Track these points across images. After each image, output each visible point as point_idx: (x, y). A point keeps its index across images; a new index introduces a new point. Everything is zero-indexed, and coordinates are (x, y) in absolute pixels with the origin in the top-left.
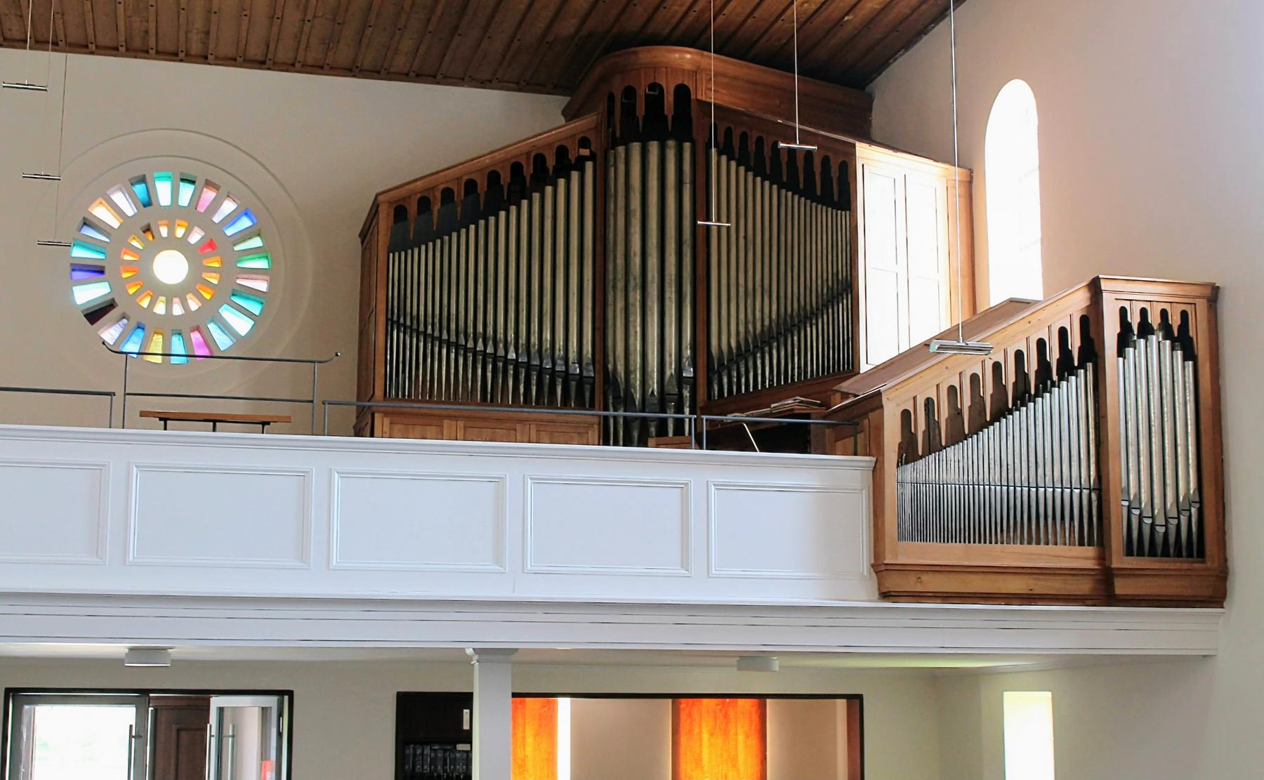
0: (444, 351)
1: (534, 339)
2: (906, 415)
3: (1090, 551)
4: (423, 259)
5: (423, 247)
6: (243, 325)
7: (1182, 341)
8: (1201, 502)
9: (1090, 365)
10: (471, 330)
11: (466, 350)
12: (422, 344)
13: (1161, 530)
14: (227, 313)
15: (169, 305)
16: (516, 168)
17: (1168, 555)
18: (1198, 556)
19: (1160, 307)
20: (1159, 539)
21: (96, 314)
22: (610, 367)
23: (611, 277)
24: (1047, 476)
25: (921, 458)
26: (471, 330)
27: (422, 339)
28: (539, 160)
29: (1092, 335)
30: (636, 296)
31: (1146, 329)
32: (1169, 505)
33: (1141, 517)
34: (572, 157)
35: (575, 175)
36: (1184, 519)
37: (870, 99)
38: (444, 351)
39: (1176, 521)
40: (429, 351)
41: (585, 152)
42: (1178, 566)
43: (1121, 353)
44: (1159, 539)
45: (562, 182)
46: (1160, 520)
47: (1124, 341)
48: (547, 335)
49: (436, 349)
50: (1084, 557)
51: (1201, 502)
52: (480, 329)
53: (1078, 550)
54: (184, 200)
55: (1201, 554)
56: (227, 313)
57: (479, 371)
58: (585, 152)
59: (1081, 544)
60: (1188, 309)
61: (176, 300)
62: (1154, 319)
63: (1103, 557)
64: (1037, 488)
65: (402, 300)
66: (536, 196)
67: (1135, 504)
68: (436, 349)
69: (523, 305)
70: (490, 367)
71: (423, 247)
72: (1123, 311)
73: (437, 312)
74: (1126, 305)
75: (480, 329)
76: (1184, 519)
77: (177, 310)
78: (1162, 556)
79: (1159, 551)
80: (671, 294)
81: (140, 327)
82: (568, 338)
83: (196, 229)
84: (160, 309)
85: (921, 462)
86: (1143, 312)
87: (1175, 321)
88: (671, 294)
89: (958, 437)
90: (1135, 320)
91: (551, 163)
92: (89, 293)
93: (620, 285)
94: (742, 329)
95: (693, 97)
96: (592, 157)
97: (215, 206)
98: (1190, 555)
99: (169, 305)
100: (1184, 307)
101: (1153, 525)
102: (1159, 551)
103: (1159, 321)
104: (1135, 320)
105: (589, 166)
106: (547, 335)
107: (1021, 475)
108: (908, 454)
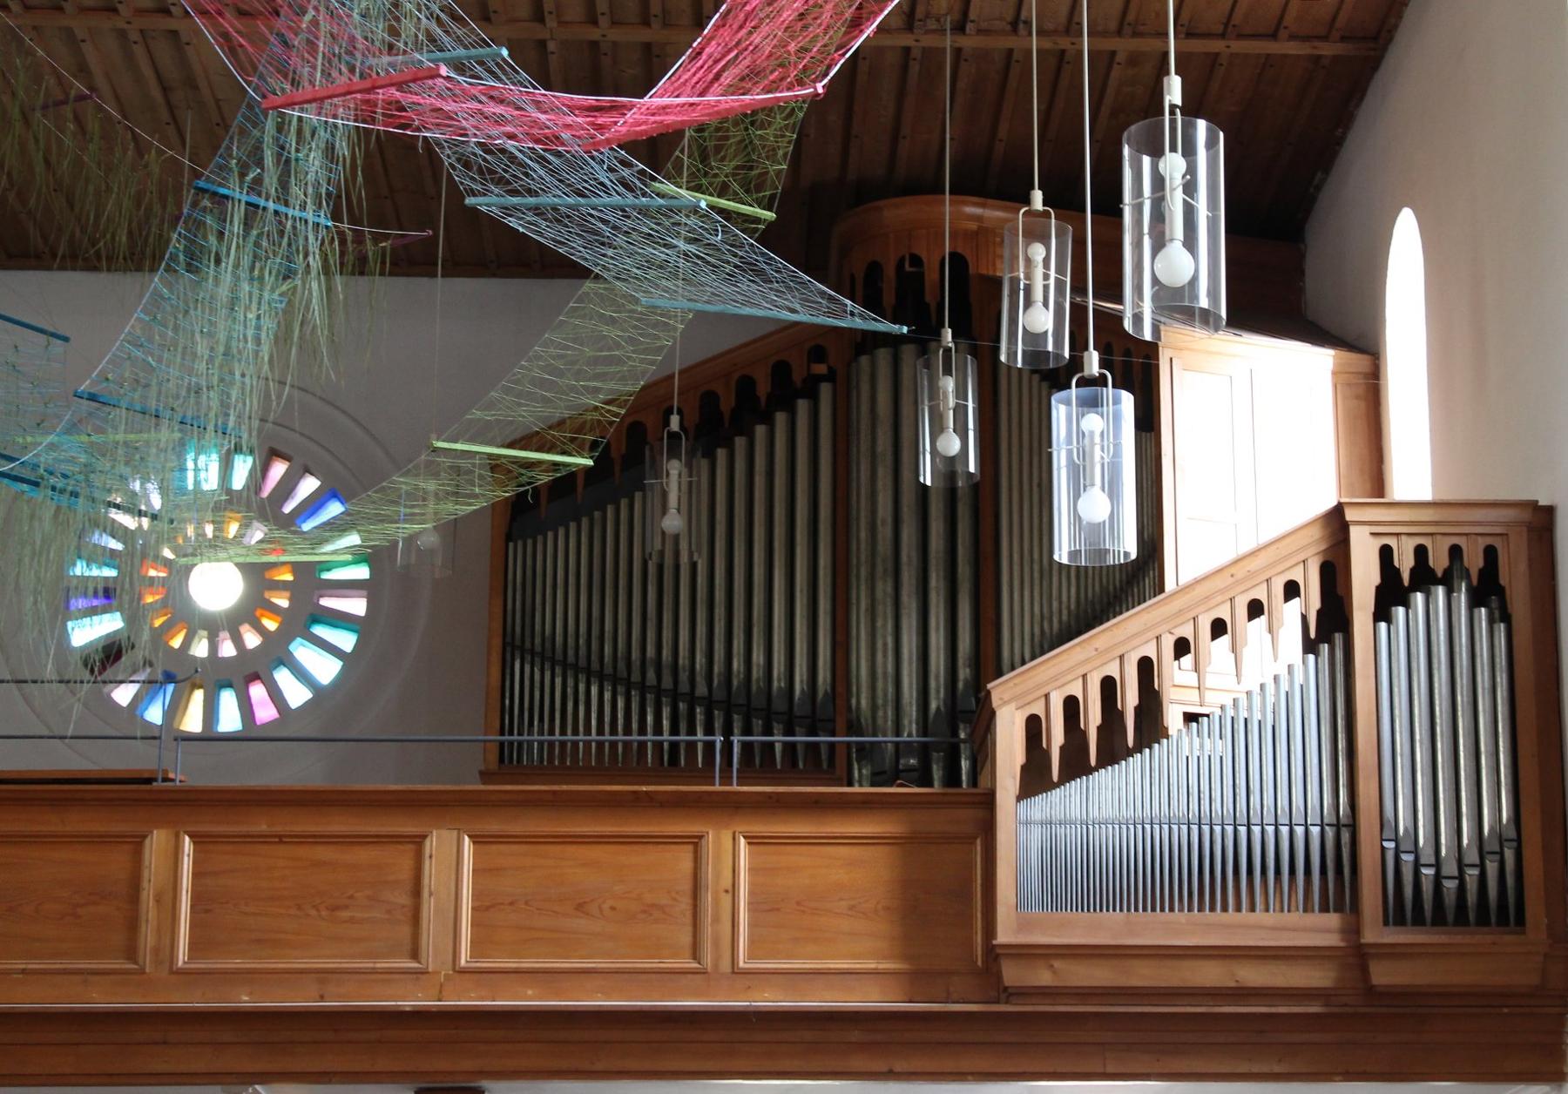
0: (594, 690)
1: (737, 664)
2: (1034, 727)
3: (1333, 919)
4: (562, 550)
5: (561, 532)
6: (326, 669)
7: (1488, 590)
8: (1519, 839)
9: (1338, 638)
10: (635, 654)
11: (659, 692)
12: (558, 681)
13: (1450, 885)
14: (302, 651)
15: (238, 640)
16: (746, 386)
17: (1466, 923)
18: (1499, 924)
19: (1482, 543)
20: (1450, 899)
21: (110, 654)
22: (854, 701)
23: (854, 561)
24: (1264, 802)
25: (1058, 785)
26: (635, 654)
27: (558, 670)
28: (746, 386)
29: (1340, 591)
30: (884, 588)
31: (1424, 577)
32: (1465, 841)
33: (1417, 865)
34: (797, 377)
35: (802, 405)
36: (1492, 868)
37: (1302, 257)
38: (594, 690)
39: (1476, 872)
40: (570, 691)
41: (821, 369)
42: (1458, 939)
43: (1382, 613)
44: (1450, 899)
45: (781, 418)
46: (1450, 868)
47: (1391, 594)
48: (758, 657)
49: (582, 687)
50: (1322, 929)
51: (1519, 839)
52: (651, 651)
53: (1318, 919)
54: (239, 480)
55: (1521, 921)
56: (302, 651)
57: (650, 719)
58: (821, 369)
59: (1324, 908)
60: (1498, 543)
61: (224, 635)
62: (1439, 561)
63: (1353, 930)
64: (1249, 826)
65: (529, 613)
66: (740, 442)
67: (1407, 845)
68: (582, 687)
69: (720, 611)
70: (666, 712)
71: (561, 532)
72: (1386, 553)
73: (583, 629)
74: (1392, 542)
75: (651, 651)
76: (1492, 868)
77: (228, 650)
78: (1434, 924)
79: (1450, 917)
80: (936, 582)
81: (169, 678)
82: (790, 660)
83: (256, 524)
84: (200, 649)
85: (1056, 794)
86: (1421, 552)
87: (1474, 561)
88: (936, 582)
89: (1113, 752)
90: (1405, 562)
91: (763, 389)
92: (87, 632)
93: (863, 572)
94: (1037, 631)
95: (972, 270)
96: (831, 377)
97: (287, 487)
98: (1503, 919)
99: (238, 640)
100: (1489, 541)
101: (1438, 877)
102: (1450, 917)
103: (1481, 563)
104: (1405, 562)
105: (825, 390)
106: (758, 657)
107: (1221, 806)
108: (1035, 779)
